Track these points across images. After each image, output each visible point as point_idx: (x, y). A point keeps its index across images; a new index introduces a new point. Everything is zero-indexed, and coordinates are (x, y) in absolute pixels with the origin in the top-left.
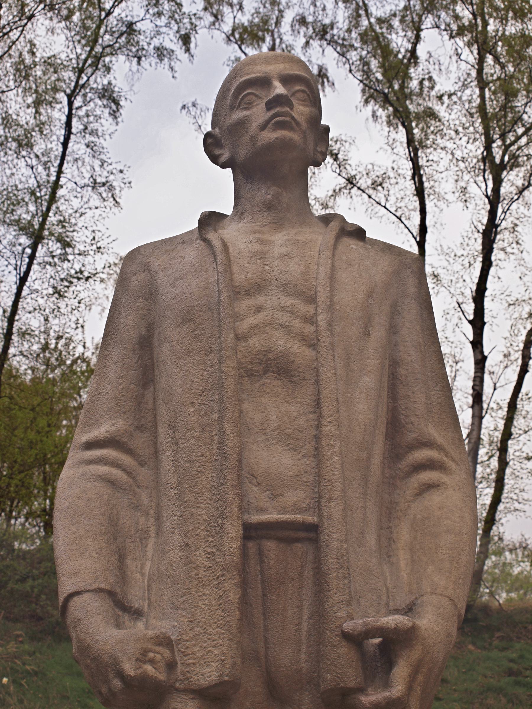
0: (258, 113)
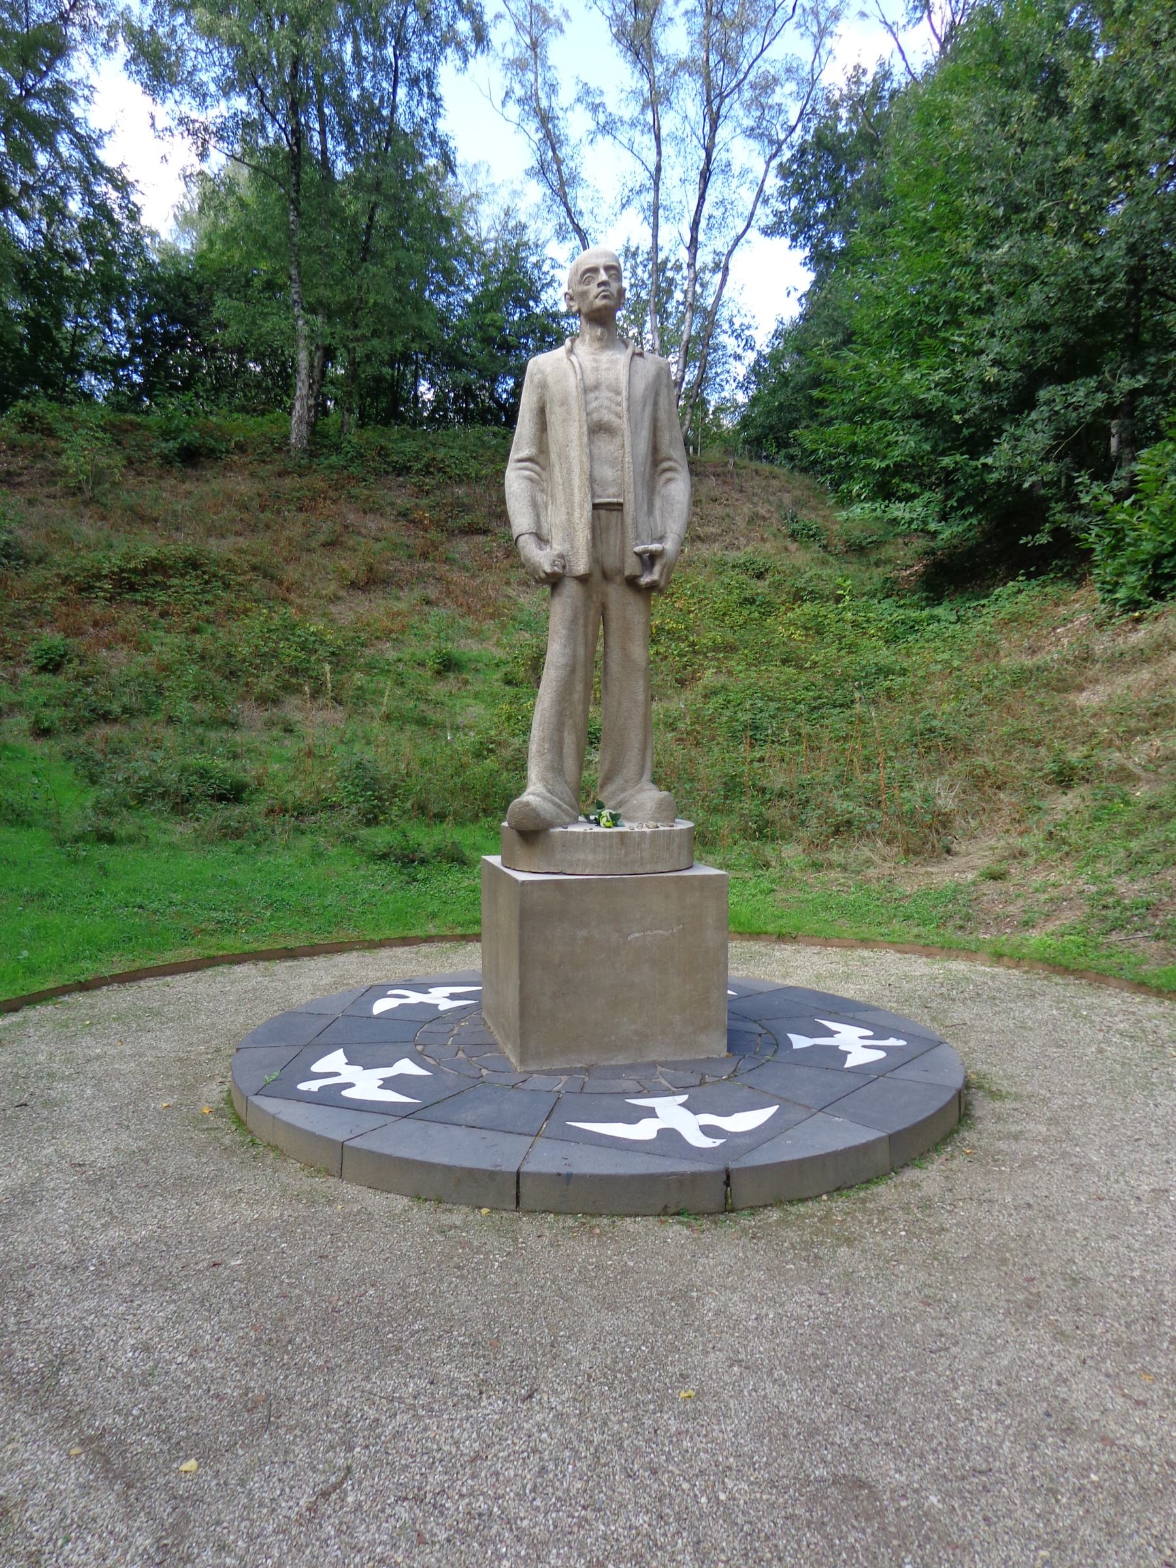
0: (594, 289)
